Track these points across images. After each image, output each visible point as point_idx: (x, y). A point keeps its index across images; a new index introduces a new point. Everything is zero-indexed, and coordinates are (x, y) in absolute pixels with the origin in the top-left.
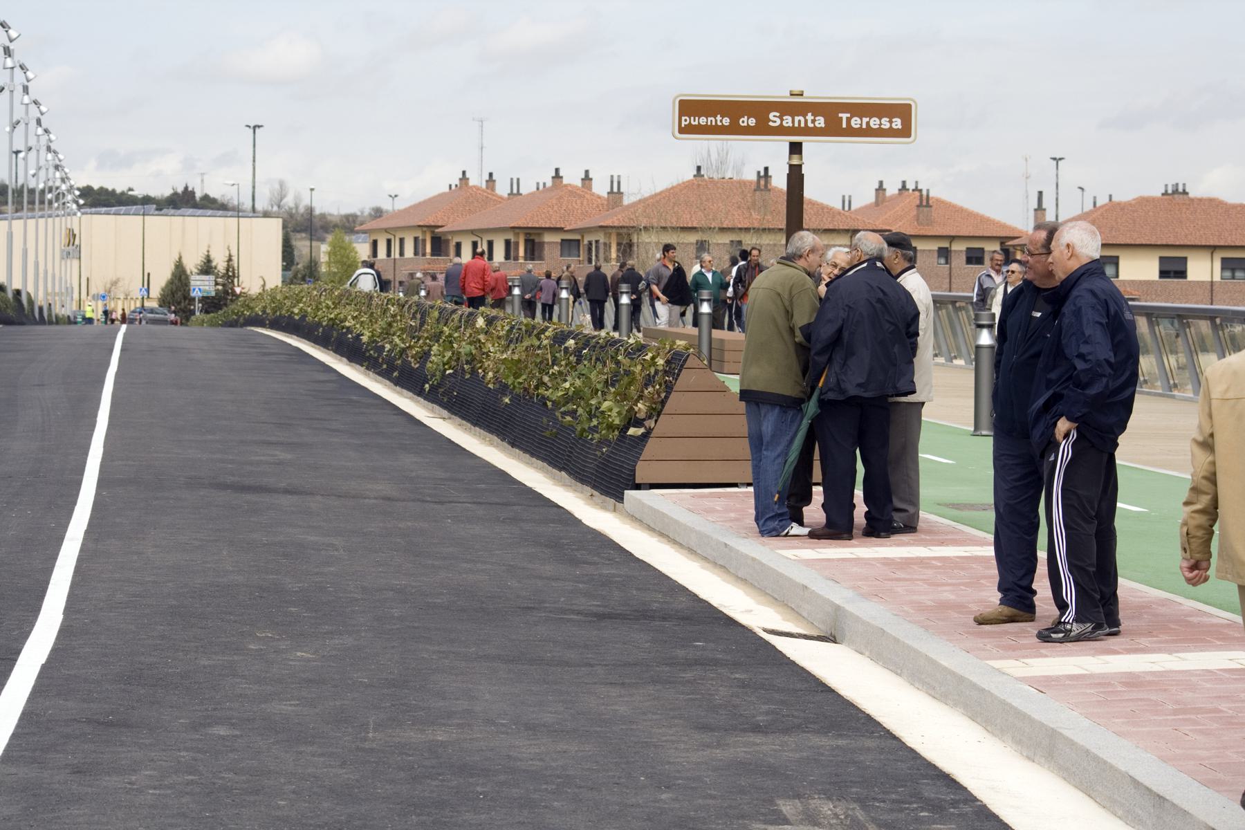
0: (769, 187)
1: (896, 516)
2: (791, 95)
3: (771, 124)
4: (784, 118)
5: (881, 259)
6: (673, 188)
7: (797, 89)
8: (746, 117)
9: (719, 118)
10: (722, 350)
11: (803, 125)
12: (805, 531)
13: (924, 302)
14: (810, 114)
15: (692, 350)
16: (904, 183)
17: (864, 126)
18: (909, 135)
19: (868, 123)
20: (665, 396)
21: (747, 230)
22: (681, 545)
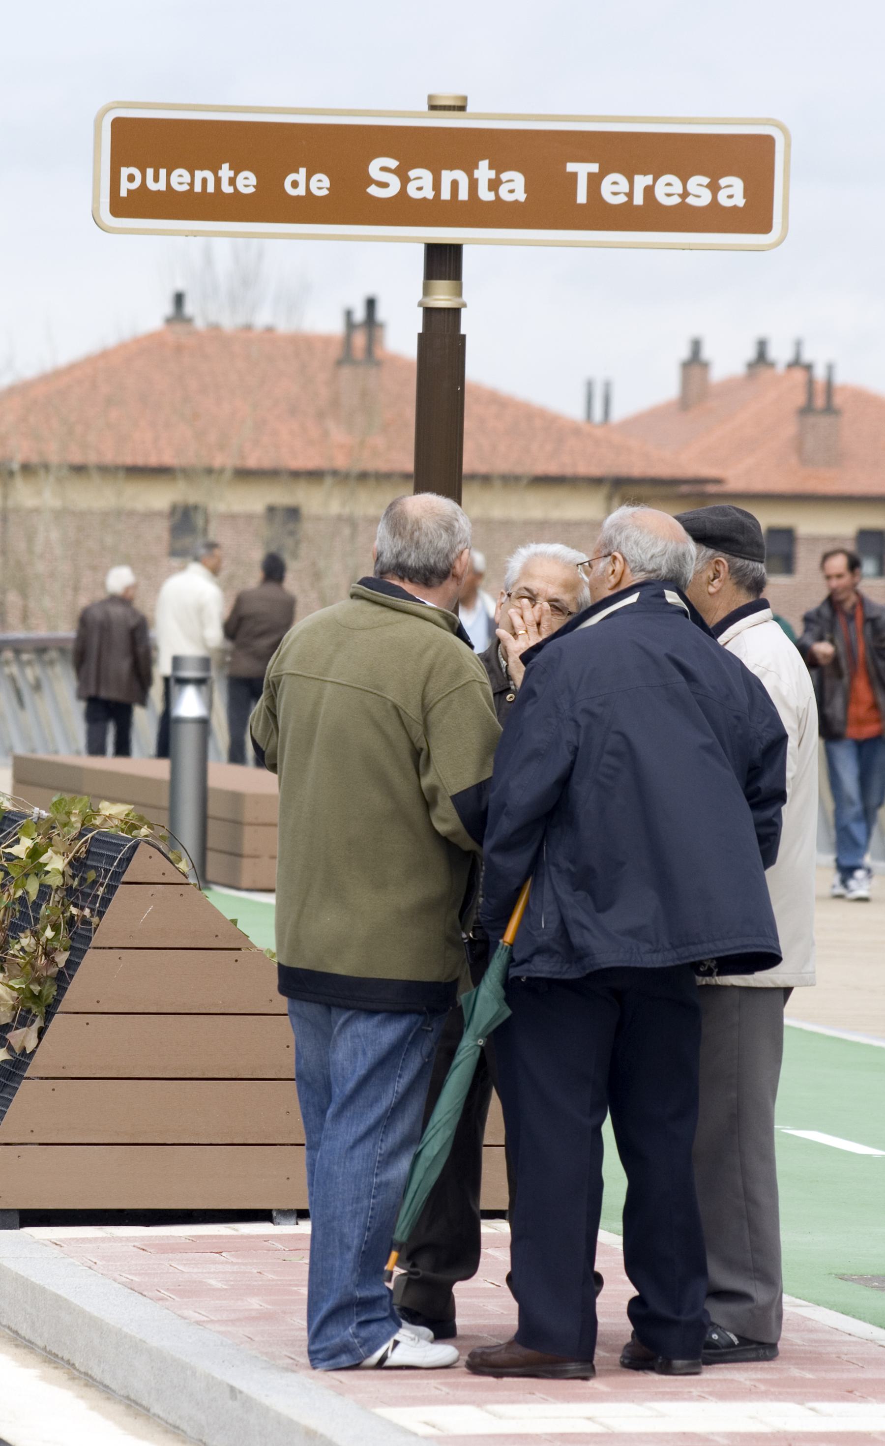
0: (378, 353)
1: (717, 1311)
2: (433, 108)
3: (373, 190)
4: (413, 174)
5: (676, 582)
6: (105, 355)
7: (447, 92)
8: (303, 171)
9: (225, 172)
10: (237, 824)
11: (463, 195)
12: (445, 1352)
13: (793, 704)
14: (484, 164)
15: (144, 831)
16: (762, 347)
17: (638, 200)
18: (765, 226)
19: (649, 191)
20: (68, 961)
21: (314, 476)
22: (105, 1390)
